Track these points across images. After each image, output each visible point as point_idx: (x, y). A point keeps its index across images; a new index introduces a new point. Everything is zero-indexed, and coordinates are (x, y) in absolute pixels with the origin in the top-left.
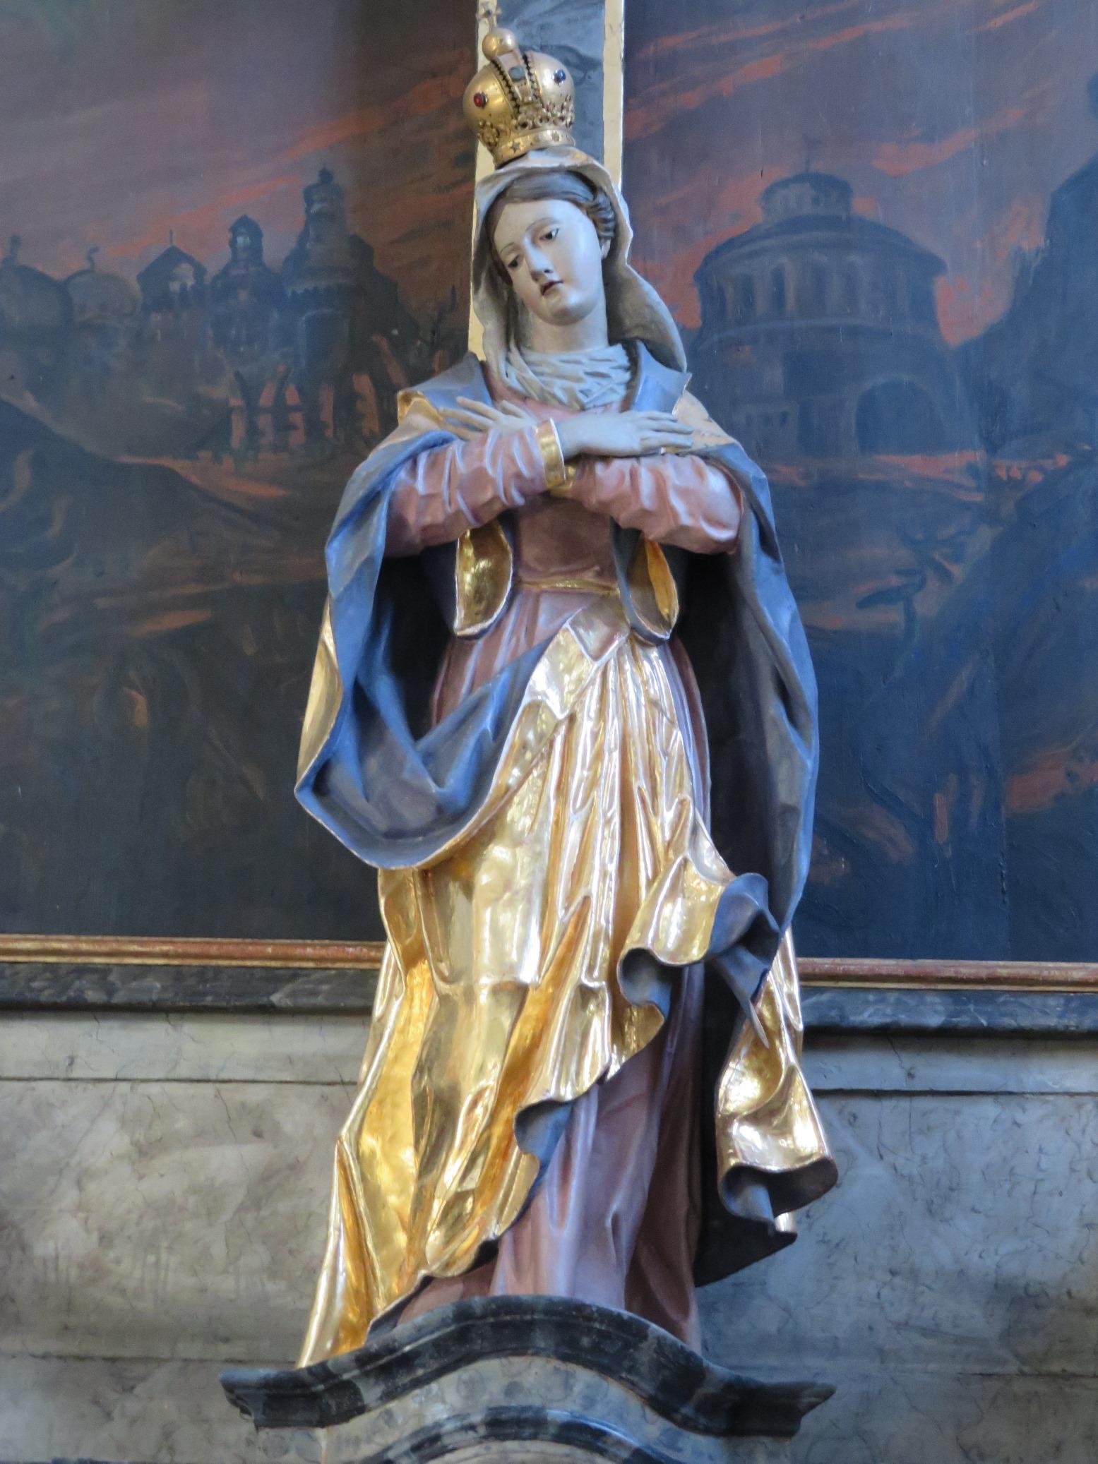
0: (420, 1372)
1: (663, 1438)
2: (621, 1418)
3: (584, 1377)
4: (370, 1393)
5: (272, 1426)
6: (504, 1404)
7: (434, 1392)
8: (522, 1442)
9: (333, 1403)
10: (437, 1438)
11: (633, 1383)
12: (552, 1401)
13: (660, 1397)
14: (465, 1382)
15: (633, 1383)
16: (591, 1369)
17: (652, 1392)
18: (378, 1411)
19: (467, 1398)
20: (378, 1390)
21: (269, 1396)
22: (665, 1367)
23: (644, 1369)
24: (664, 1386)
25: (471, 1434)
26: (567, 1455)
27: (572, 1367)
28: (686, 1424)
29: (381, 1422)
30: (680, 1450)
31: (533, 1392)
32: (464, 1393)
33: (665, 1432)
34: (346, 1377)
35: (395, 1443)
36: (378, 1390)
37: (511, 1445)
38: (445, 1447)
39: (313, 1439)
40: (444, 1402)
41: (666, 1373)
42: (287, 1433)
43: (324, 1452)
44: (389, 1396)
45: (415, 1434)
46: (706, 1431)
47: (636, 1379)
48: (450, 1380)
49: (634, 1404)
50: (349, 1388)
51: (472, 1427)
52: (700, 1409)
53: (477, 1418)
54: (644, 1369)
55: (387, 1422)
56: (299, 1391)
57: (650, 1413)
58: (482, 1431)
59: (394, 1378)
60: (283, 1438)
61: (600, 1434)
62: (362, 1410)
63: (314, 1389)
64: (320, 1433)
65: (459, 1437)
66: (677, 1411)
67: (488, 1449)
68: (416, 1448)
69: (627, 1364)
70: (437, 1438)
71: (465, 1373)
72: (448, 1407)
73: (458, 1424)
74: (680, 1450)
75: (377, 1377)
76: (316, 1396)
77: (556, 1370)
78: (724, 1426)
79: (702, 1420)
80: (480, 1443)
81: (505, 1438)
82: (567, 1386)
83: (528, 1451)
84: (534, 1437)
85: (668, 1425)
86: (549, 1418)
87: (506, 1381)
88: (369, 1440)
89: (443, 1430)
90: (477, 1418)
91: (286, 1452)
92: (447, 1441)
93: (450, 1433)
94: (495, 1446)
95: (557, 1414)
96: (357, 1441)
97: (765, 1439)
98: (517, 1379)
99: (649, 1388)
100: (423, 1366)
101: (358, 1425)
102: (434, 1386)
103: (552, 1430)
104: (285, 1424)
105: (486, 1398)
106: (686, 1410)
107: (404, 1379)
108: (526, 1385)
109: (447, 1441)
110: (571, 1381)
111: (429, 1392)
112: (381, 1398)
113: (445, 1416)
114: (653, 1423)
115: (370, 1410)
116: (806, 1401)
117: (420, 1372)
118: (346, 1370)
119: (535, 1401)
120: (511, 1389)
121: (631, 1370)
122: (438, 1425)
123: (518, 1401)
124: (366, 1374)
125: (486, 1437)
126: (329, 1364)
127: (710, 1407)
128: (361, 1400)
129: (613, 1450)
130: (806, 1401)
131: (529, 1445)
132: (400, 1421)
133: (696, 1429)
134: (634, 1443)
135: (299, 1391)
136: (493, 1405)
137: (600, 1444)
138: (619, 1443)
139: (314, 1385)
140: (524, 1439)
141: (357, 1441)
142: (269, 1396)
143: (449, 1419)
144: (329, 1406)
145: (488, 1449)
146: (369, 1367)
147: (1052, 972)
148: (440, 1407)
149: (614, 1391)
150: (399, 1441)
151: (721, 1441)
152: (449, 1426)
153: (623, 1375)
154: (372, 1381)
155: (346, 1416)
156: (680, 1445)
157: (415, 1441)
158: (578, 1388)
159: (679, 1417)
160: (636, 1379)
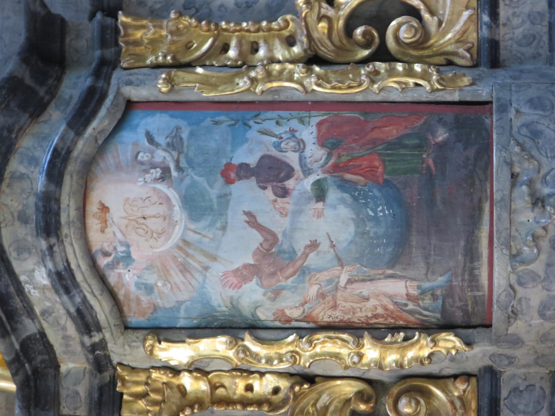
0: (12, 289)
1: (62, 108)
2: (46, 138)
3: (15, 165)
4: (29, 328)
5: (59, 404)
6: (33, 225)
7: (27, 279)
8: (62, 210)
9: (39, 358)
10: (59, 274)
11: (20, 129)
12: (32, 189)
13: (31, 109)
14: (18, 255)
15: (20, 129)
16: (8, 160)
17: (27, 115)
18: (43, 322)
19: (30, 253)
20: (27, 322)
21: (36, 406)
22: (8, 105)
23: (10, 121)
24: (23, 107)
25: (56, 248)
26: (72, 176)
27: (7, 175)
28: (53, 93)
29: (50, 319)
30: (71, 97)
31: (25, 202)
32: (26, 255)
33: (57, 107)
34: (17, 347)
35: (65, 308)
36: (27, 322)
37: (63, 219)
38: (65, 268)
39: (69, 372)
40: (33, 270)
41: (12, 104)
42: (63, 393)
43: (77, 366)
44: (30, 312)
45: (57, 292)
46: (59, 80)
47: (17, 127)
48: (18, 267)
49: (36, 128)
50: (26, 345)
51: (51, 248)
52: (42, 84)
53: (43, 244)
54: (10, 121)
55: (50, 315)
56: (32, 384)
57: (44, 117)
58: (53, 240)
59: (17, 309)
60: (68, 396)
61: (56, 153)
62: (43, 334)
63: (30, 373)
64: (63, 368)
65: (58, 259)
66: (42, 98)
67: (66, 236)
68: (67, 291)
69: (5, 133)
70: (59, 274)
71: (12, 255)
72: (36, 267)
73: (48, 258)
74: (71, 97)
75: (16, 322)
76: (35, 371)
77: (9, 186)
78: (57, 68)
79: (50, 81)
80: (62, 241)
81: (58, 224)
82: (22, 177)
83: (68, 205)
84: (58, 201)
85: (52, 104)
86: (43, 190)
87: (17, 223)
88: (64, 329)
89: (53, 270)
90: (43, 244)
91: (77, 393)
92: (61, 267)
93: (55, 264)
94: (65, 230)
95: (40, 182)
96: (66, 338)
97: (67, 40)
98: (16, 215)
99: (25, 118)
100: (7, 286)
101: (54, 337)
102: (23, 278)
103: (52, 187)
104: (57, 395)
105: (29, 239)
106: (42, 92)
107: (17, 302)
108: (20, 207)
109: (61, 267)
110: (18, 174)
111: (27, 283)
112: (33, 320)
113: (43, 269)
114: (51, 116)
115: (42, 328)
116: (39, 9)
117: (12, 289)
118: (12, 345)
119: (32, 200)
120: (23, 219)
121: (10, 131)
122: (49, 274)
123: (31, 212)
124: (14, 330)
125: (58, 237)
126: (7, 359)
127: (41, 77)
128: (35, 334)
129: (68, 143)
130: (39, 9)
131: (63, 206)
132: (48, 304)
133: (57, 87)
134: (63, 127)
135: (32, 384)
136: (35, 233)
137: (63, 153)
138: (62, 138)
139: (26, 372)
140: (59, 208)
141: (66, 338)
142: (36, 406)
143: (45, 266)
144: (42, 362)
145: (66, 236)
146: (9, 328)
147: (97, 293)
148: (37, 273)
149: (26, 143)
150: (63, 304)
151: (68, 72)
152: (50, 265)
153: (14, 136)
154: (19, 326)
155: (49, 348)
156: (67, 97)
157: (62, 292)
158: (22, 169)
159: (47, 98)
160: (17, 127)
